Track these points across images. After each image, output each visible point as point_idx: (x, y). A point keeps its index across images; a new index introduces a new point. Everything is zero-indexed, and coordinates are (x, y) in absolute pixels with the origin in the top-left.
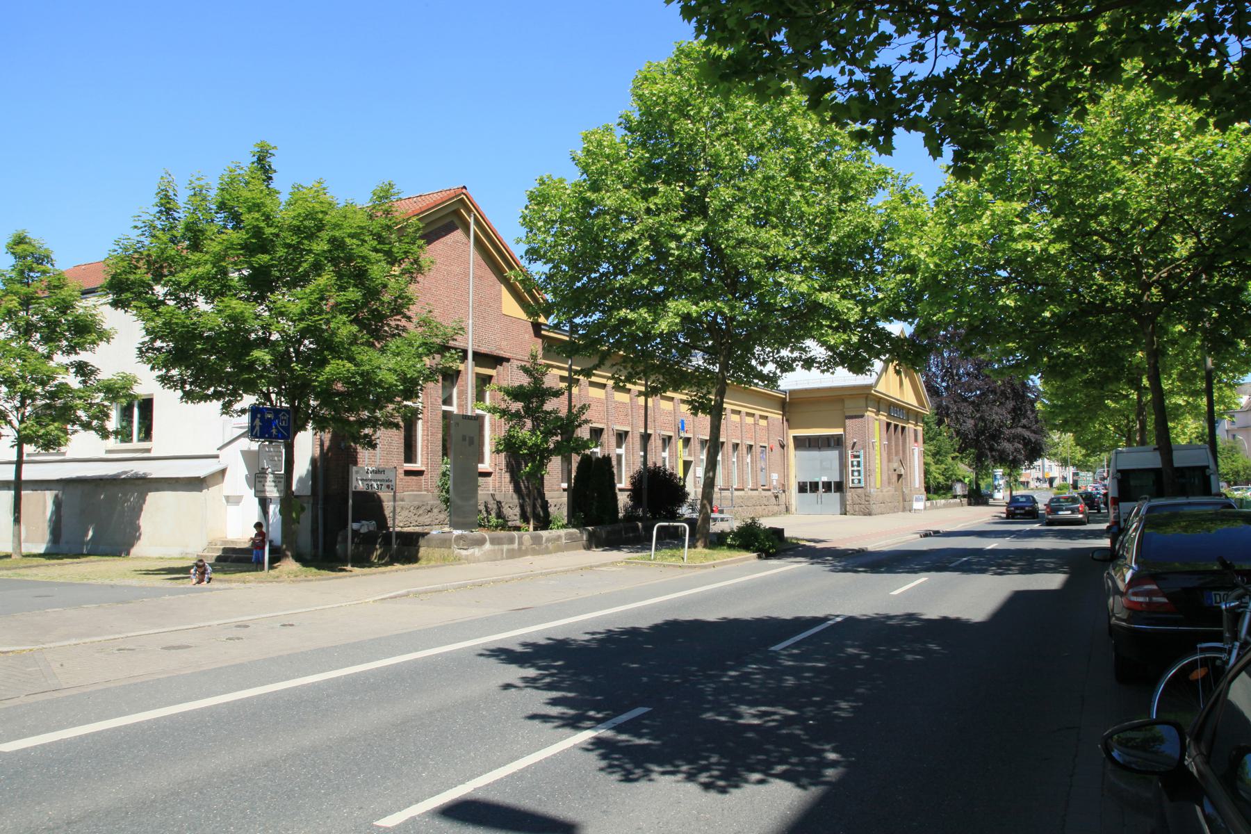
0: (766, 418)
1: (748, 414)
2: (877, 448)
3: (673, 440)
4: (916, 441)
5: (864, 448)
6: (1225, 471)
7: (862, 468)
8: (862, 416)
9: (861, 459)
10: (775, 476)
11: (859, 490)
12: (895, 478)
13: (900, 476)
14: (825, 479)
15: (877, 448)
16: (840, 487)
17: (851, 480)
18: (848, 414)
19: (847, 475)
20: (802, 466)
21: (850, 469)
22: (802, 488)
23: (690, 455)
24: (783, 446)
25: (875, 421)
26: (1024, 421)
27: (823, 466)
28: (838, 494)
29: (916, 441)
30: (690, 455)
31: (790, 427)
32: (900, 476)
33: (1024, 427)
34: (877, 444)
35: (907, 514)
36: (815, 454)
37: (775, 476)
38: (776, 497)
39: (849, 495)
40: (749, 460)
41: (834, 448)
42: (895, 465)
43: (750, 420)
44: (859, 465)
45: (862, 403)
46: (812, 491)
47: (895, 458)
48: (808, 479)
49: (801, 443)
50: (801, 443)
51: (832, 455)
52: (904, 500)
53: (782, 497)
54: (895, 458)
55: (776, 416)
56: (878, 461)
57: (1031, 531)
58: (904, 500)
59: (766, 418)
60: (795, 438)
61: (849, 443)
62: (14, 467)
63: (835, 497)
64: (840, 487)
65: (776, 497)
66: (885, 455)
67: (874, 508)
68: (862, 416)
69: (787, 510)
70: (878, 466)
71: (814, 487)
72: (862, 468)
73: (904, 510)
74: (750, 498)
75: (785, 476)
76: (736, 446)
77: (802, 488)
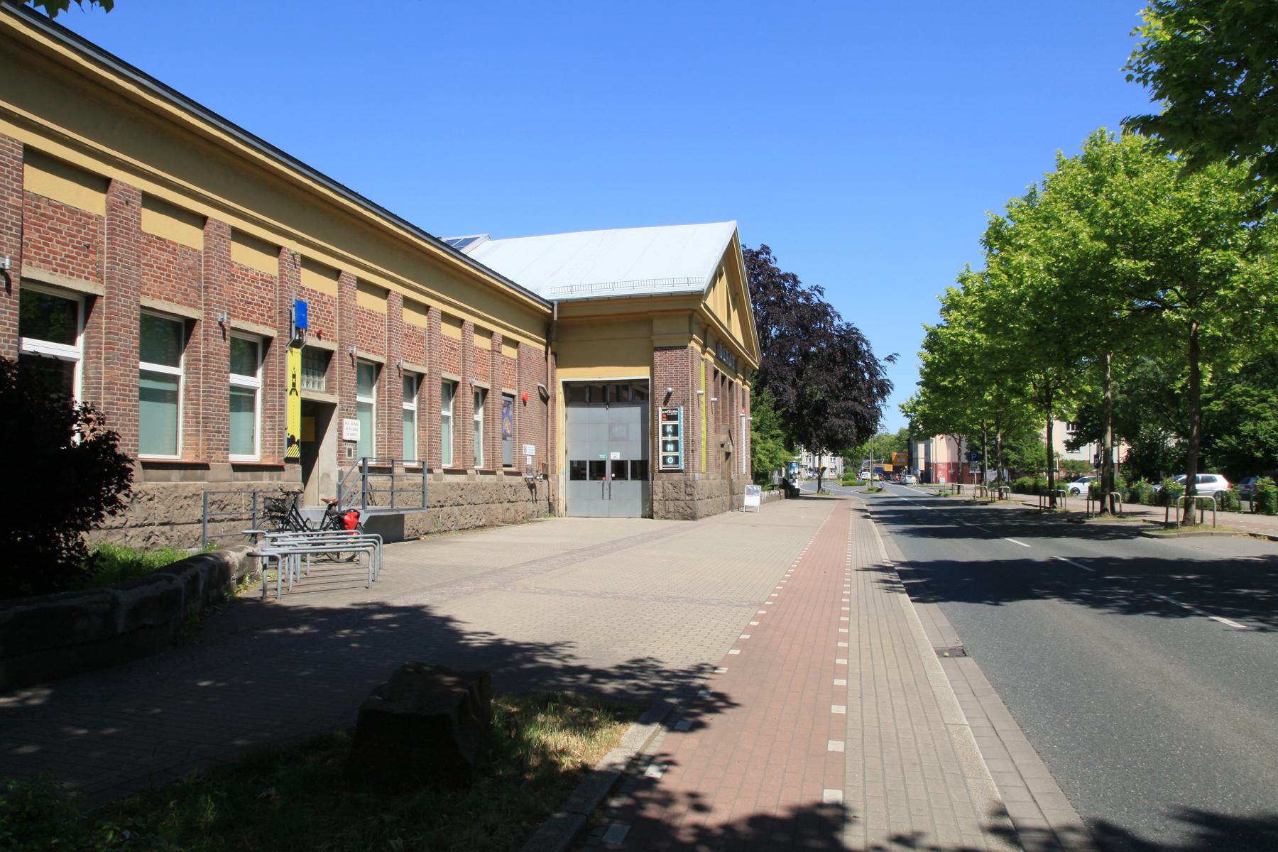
0: (515, 344)
1: (479, 330)
2: (703, 406)
3: (275, 347)
4: (744, 406)
5: (684, 403)
6: (1030, 461)
7: (681, 438)
8: (685, 347)
9: (680, 422)
10: (530, 450)
11: (676, 476)
12: (722, 456)
13: (728, 454)
14: (616, 456)
15: (703, 406)
16: (641, 470)
17: (663, 456)
18: (657, 344)
19: (655, 449)
20: (575, 433)
21: (661, 438)
22: (577, 472)
23: (330, 390)
24: (545, 399)
25: (700, 360)
26: (855, 393)
27: (615, 434)
28: (638, 483)
29: (744, 406)
30: (330, 390)
31: (559, 365)
32: (728, 454)
33: (855, 400)
34: (703, 399)
35: (736, 512)
36: (599, 412)
37: (530, 450)
38: (532, 487)
39: (659, 485)
40: (479, 417)
41: (631, 403)
42: (724, 437)
43: (482, 342)
44: (675, 433)
45: (683, 325)
46: (593, 478)
47: (722, 427)
48: (587, 456)
49: (578, 394)
50: (578, 394)
51: (630, 415)
52: (732, 493)
53: (542, 487)
54: (722, 427)
55: (534, 345)
56: (704, 429)
57: (1053, 565)
58: (732, 493)
59: (515, 344)
60: (566, 384)
61: (660, 394)
62: (1163, 520)
63: (633, 487)
64: (641, 470)
65: (532, 487)
66: (712, 419)
67: (701, 507)
68: (685, 347)
69: (551, 509)
70: (704, 436)
71: (598, 470)
72: (681, 438)
73: (732, 507)
74: (476, 489)
75: (548, 449)
76: (451, 388)
77: (577, 472)
